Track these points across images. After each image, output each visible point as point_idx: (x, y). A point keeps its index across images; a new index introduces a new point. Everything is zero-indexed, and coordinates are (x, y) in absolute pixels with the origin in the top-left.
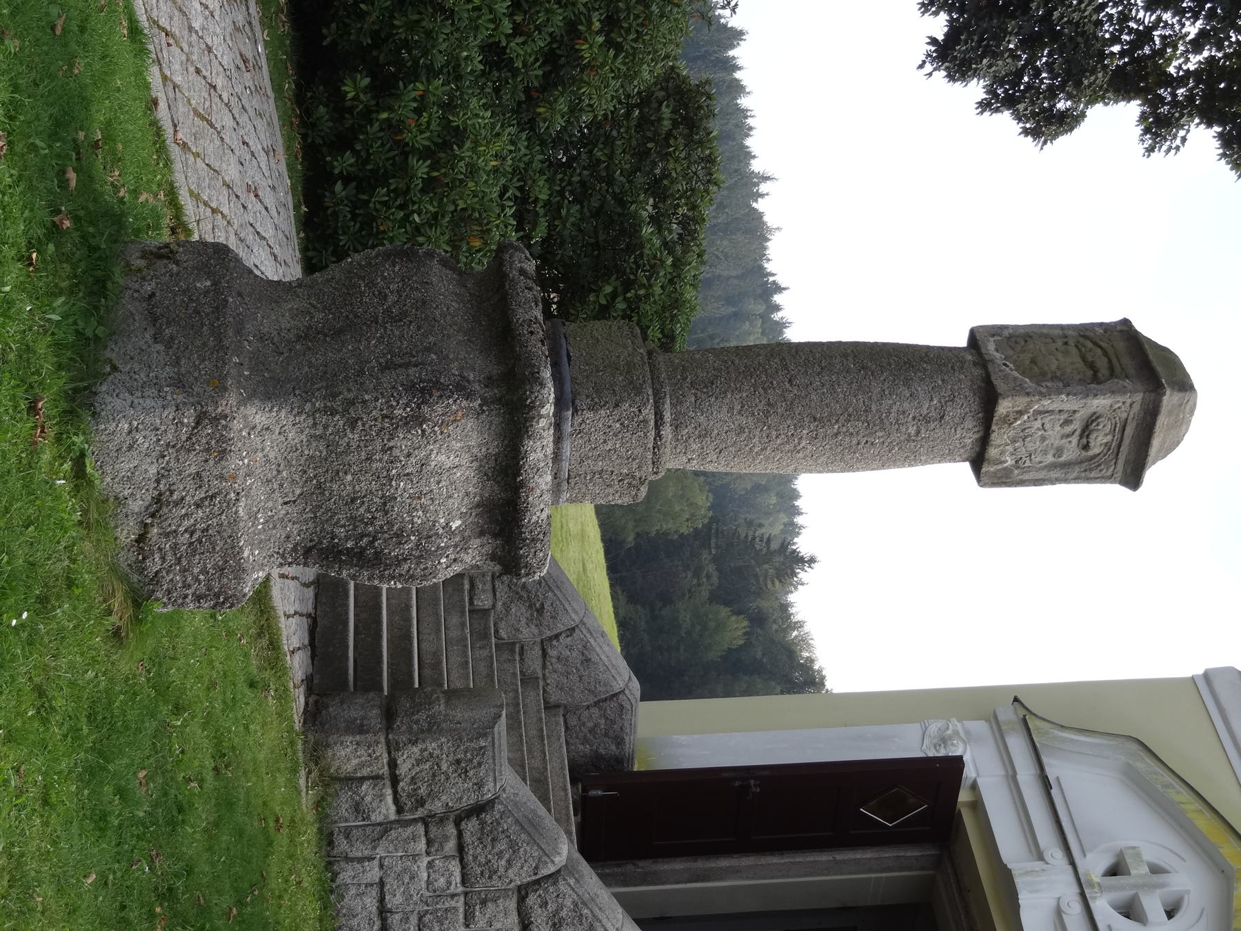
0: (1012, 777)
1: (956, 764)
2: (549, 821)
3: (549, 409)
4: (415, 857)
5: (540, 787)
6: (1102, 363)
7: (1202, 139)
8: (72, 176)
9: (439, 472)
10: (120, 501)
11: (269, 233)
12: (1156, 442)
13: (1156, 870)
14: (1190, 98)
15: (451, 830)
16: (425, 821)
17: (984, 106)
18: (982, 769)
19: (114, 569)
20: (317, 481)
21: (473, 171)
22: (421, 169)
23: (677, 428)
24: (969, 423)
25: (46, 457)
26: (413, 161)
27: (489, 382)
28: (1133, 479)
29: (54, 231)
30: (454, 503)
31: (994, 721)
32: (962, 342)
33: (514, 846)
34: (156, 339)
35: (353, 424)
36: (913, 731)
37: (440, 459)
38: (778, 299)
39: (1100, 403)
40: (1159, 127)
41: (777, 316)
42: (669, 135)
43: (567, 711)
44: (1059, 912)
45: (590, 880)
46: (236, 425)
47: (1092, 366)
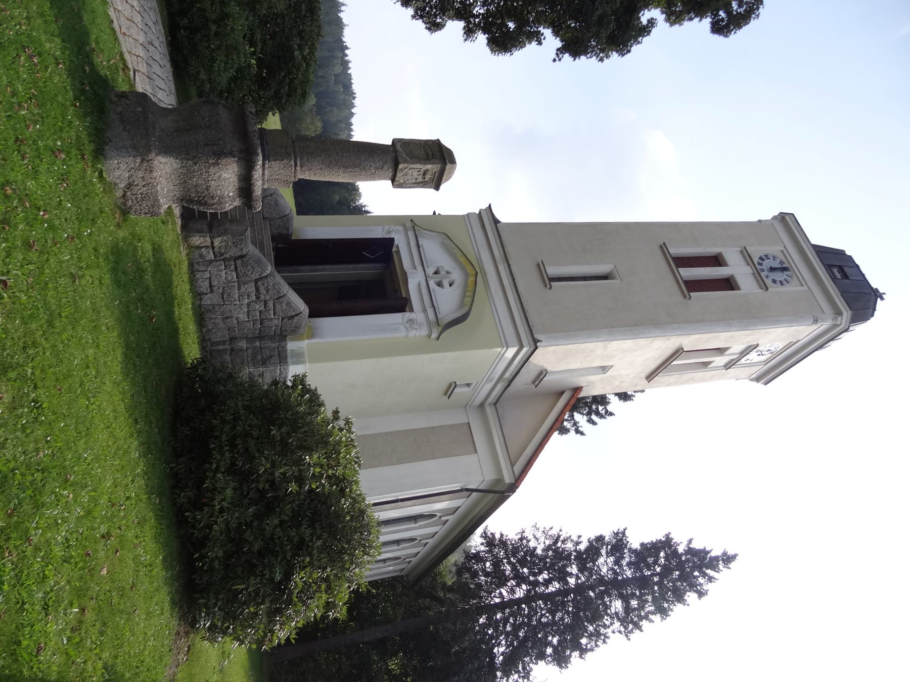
0: (409, 244)
1: (392, 240)
2: (265, 260)
3: (260, 162)
4: (221, 271)
5: (262, 249)
6: (430, 153)
7: (481, 38)
8: (87, 68)
9: (225, 179)
10: (116, 184)
11: (157, 57)
12: (444, 178)
13: (448, 273)
14: (480, 22)
15: (233, 263)
16: (224, 260)
17: (413, 17)
18: (400, 241)
19: (116, 204)
20: (184, 179)
21: (233, 30)
22: (214, 28)
23: (301, 167)
24: (390, 170)
25: (89, 172)
26: (210, 24)
27: (241, 151)
28: (437, 188)
29: (83, 92)
30: (230, 188)
31: (404, 226)
32: (390, 143)
33: (253, 268)
34: (124, 129)
35: (195, 164)
36: (380, 229)
37: (225, 175)
38: (347, 52)
39: (429, 167)
40: (469, 32)
41: (347, 58)
42: (305, 16)
43: (270, 220)
44: (419, 285)
45: (278, 278)
46: (155, 162)
47: (427, 154)
